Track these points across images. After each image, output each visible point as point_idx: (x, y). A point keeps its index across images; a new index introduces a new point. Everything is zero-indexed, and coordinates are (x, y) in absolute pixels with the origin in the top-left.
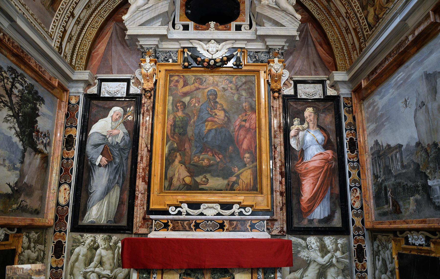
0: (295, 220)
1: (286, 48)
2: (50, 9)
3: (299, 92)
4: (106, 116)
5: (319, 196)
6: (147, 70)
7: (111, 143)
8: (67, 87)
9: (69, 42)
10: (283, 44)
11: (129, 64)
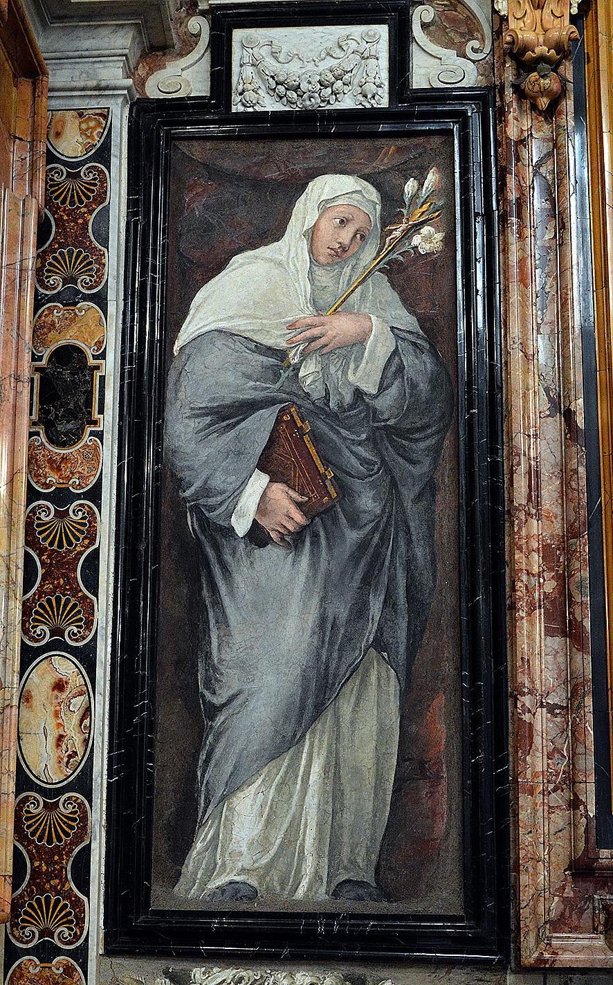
4: (271, 232)
7: (317, 394)
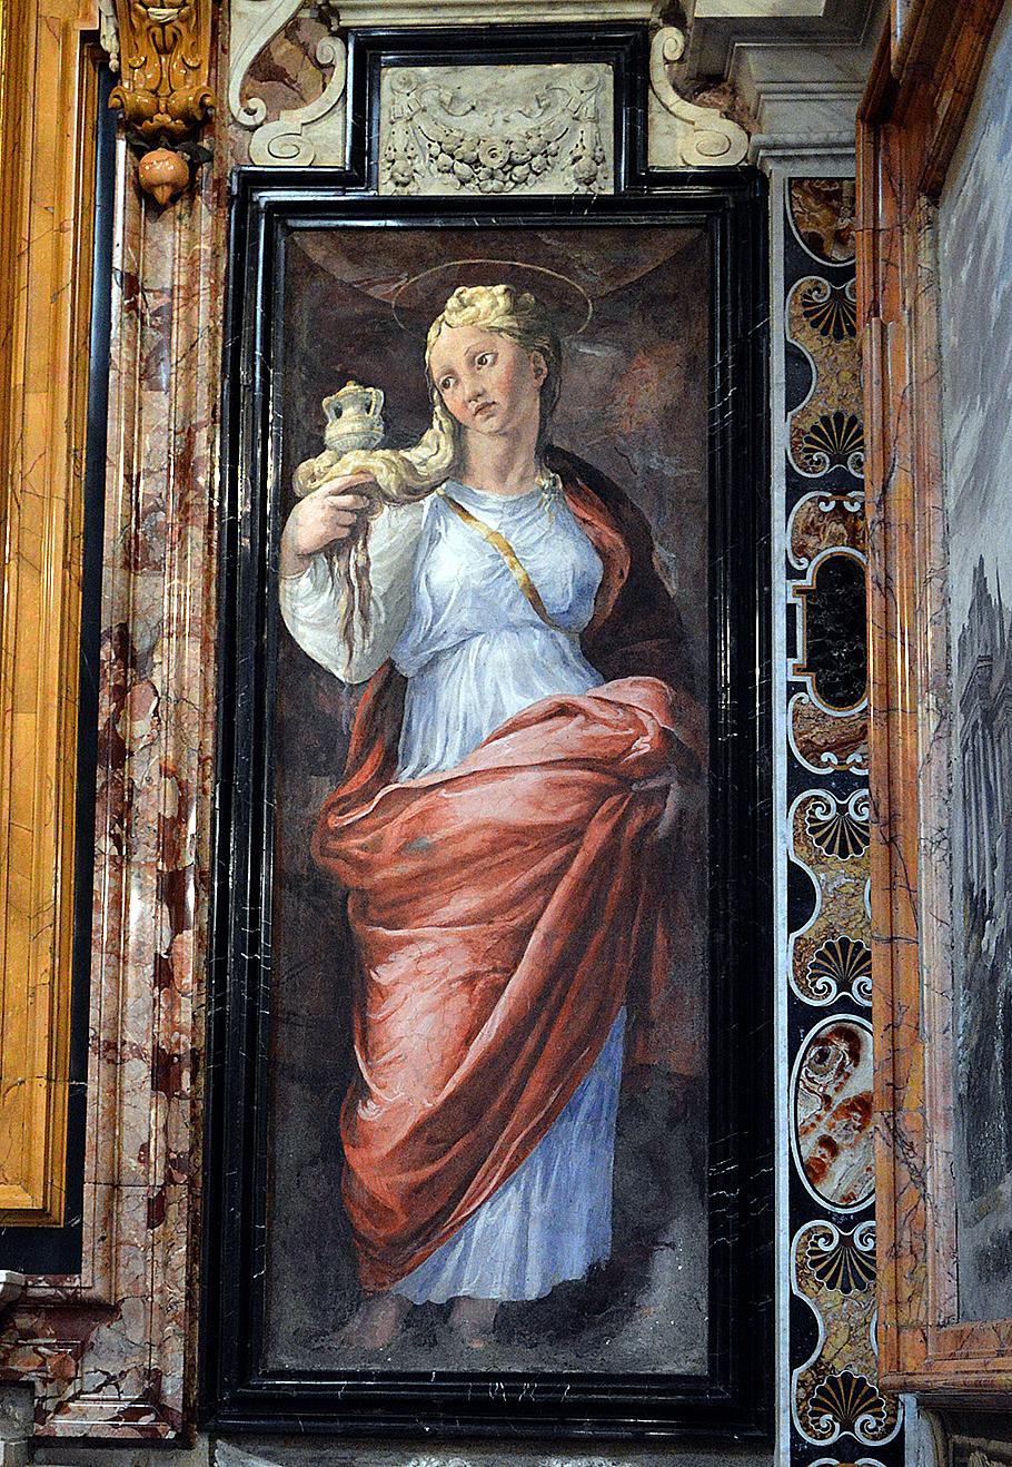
0: (289, 1313)
3: (392, 139)
5: (518, 1092)
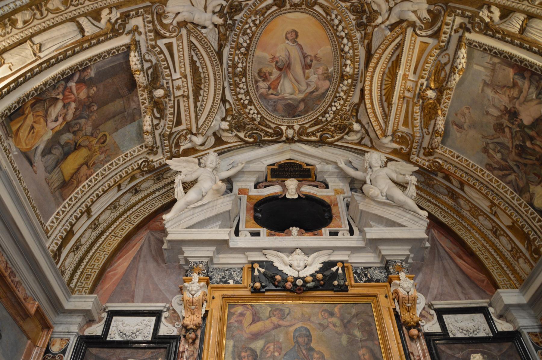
1: (410, 261)
2: (57, 194)
3: (449, 327)
6: (193, 293)
8: (51, 323)
9: (74, 251)
10: (408, 253)
11: (162, 288)
